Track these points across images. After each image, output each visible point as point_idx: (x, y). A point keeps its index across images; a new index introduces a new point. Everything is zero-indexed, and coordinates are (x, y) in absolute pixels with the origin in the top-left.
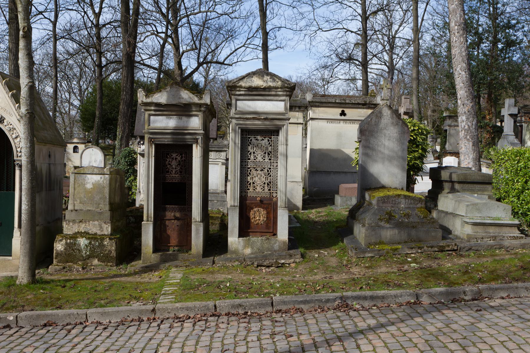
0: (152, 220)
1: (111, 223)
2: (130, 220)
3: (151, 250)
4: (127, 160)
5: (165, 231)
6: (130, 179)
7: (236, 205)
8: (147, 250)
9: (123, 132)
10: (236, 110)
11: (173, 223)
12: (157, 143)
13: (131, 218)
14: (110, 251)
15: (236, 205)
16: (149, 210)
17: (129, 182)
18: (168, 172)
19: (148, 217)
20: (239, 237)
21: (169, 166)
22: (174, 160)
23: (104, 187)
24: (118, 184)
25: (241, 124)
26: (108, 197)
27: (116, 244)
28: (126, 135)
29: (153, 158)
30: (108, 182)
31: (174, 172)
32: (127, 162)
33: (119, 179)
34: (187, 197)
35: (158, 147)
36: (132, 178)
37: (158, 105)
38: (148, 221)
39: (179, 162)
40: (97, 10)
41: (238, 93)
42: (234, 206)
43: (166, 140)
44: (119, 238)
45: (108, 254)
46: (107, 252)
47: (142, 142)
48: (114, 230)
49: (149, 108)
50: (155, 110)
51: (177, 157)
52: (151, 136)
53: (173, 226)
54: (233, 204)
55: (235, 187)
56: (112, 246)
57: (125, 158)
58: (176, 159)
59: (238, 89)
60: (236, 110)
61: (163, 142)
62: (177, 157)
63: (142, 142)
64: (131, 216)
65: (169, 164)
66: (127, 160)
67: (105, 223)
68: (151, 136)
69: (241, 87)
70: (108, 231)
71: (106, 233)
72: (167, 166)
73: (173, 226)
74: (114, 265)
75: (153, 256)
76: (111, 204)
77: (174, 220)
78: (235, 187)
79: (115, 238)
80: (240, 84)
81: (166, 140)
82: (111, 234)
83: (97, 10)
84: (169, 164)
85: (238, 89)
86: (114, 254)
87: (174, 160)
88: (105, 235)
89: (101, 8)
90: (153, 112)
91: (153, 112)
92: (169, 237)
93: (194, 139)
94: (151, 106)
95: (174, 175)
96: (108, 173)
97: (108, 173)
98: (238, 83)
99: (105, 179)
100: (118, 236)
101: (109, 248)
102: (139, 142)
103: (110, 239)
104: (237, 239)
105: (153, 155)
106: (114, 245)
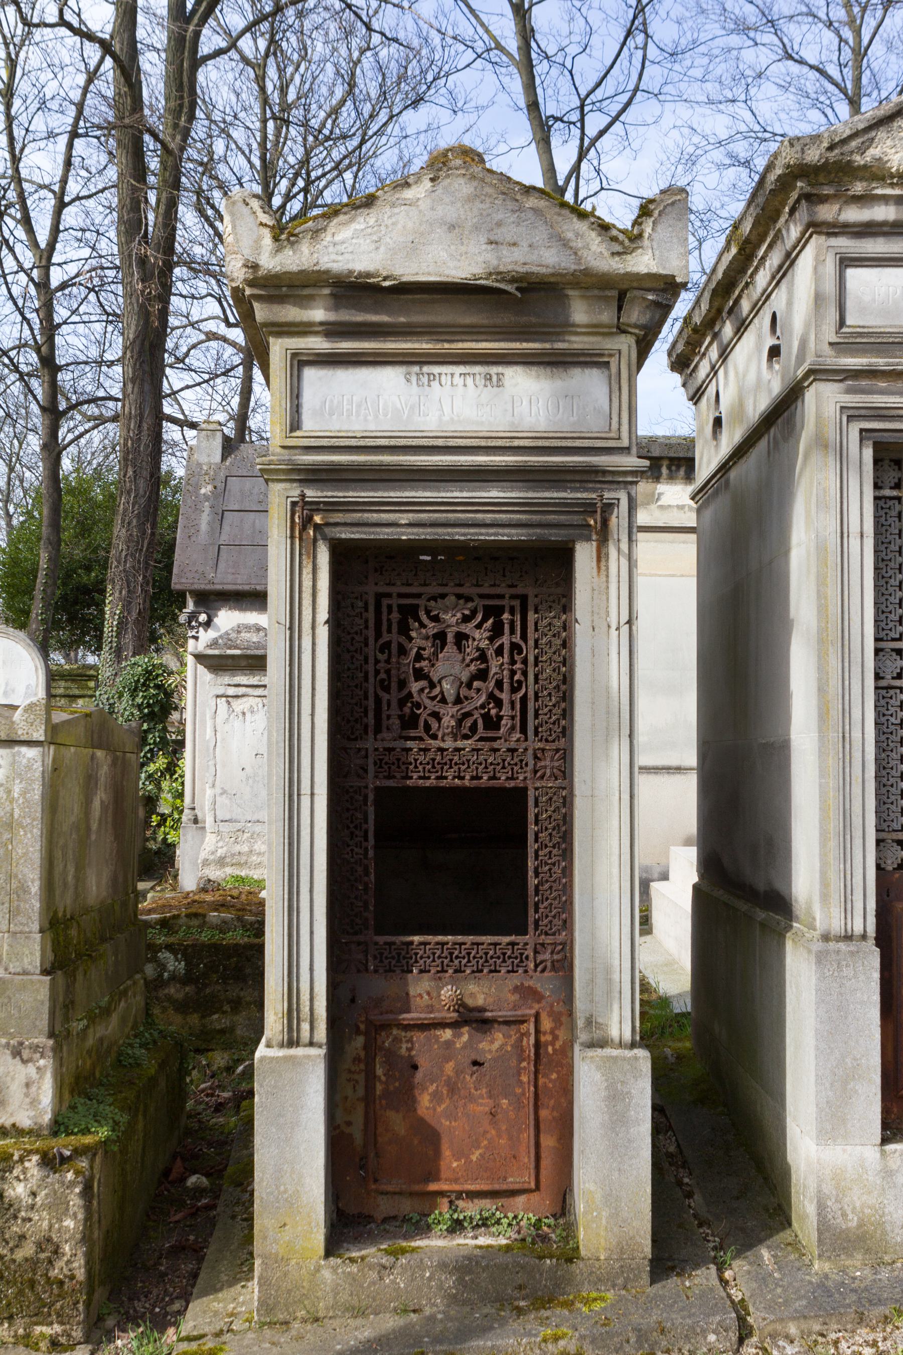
0: (321, 1034)
1: (57, 1050)
2: (163, 967)
3: (321, 1251)
4: (139, 700)
5: (405, 1096)
6: (152, 768)
7: (858, 928)
8: (286, 1235)
9: (127, 606)
10: (842, 323)
11: (449, 1044)
12: (345, 534)
13: (165, 956)
14: (49, 1246)
15: (858, 928)
16: (297, 961)
17: (150, 776)
18: (410, 722)
19: (292, 1014)
20: (885, 1141)
21: (415, 687)
22: (450, 648)
23: (10, 825)
24: (100, 797)
25: (879, 413)
26: (35, 888)
27: (87, 1192)
28: (134, 615)
29: (323, 633)
30: (36, 794)
31: (448, 721)
32: (140, 707)
33: (104, 771)
34: (532, 881)
35: (355, 565)
36: (161, 762)
37: (353, 290)
38: (292, 1042)
39: (483, 657)
40: (43, 238)
41: (854, 214)
42: (848, 938)
43: (404, 519)
44: (105, 1143)
45: (32, 1263)
46: (28, 1250)
47: (203, 617)
48: (79, 1089)
49: (292, 313)
50: (332, 331)
51: (467, 628)
52: (312, 494)
53: (449, 1067)
54: (837, 926)
55: (846, 816)
56: (58, 1207)
57: (134, 692)
58: (461, 638)
59: (859, 188)
60: (842, 323)
61: (385, 534)
62: (467, 628)
63: (203, 617)
64: (169, 947)
65: (420, 675)
66: (139, 700)
67: (16, 1053)
68: (312, 494)
69: (878, 173)
70: (34, 1102)
71: (25, 1120)
72: (402, 684)
73: (449, 1067)
74: (78, 1333)
75: (330, 1273)
76: (55, 924)
77: (454, 1025)
78: (846, 816)
79: (78, 1152)
80: (874, 152)
81: (404, 519)
82: (58, 1126)
83: (43, 238)
84: (420, 675)
85: (859, 188)
86: (73, 1262)
87: (450, 648)
88: (17, 1131)
89: (55, 231)
90: (318, 344)
91: (318, 344)
92: (430, 1137)
93: (588, 508)
94: (304, 301)
95: (449, 744)
96: (39, 734)
97: (39, 734)
98: (862, 150)
99: (16, 772)
100: (104, 1133)
101: (42, 1221)
102: (193, 616)
103: (50, 1162)
104: (871, 1153)
105: (323, 614)
106: (75, 1201)
